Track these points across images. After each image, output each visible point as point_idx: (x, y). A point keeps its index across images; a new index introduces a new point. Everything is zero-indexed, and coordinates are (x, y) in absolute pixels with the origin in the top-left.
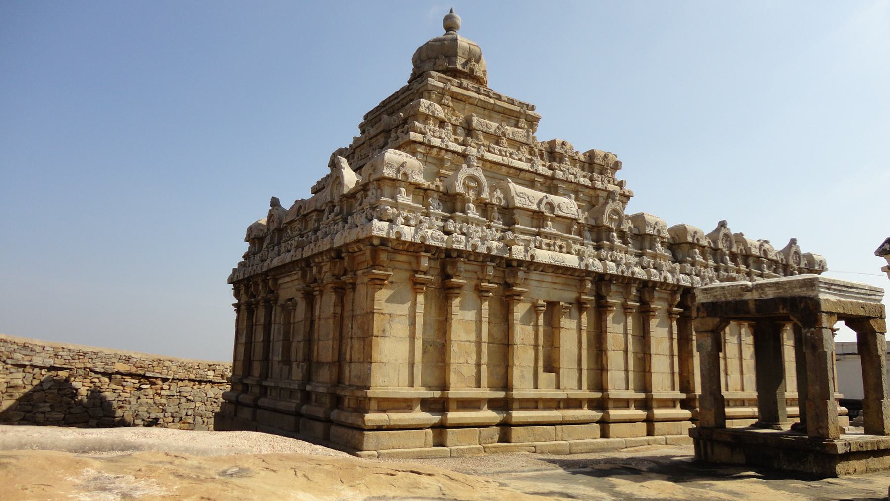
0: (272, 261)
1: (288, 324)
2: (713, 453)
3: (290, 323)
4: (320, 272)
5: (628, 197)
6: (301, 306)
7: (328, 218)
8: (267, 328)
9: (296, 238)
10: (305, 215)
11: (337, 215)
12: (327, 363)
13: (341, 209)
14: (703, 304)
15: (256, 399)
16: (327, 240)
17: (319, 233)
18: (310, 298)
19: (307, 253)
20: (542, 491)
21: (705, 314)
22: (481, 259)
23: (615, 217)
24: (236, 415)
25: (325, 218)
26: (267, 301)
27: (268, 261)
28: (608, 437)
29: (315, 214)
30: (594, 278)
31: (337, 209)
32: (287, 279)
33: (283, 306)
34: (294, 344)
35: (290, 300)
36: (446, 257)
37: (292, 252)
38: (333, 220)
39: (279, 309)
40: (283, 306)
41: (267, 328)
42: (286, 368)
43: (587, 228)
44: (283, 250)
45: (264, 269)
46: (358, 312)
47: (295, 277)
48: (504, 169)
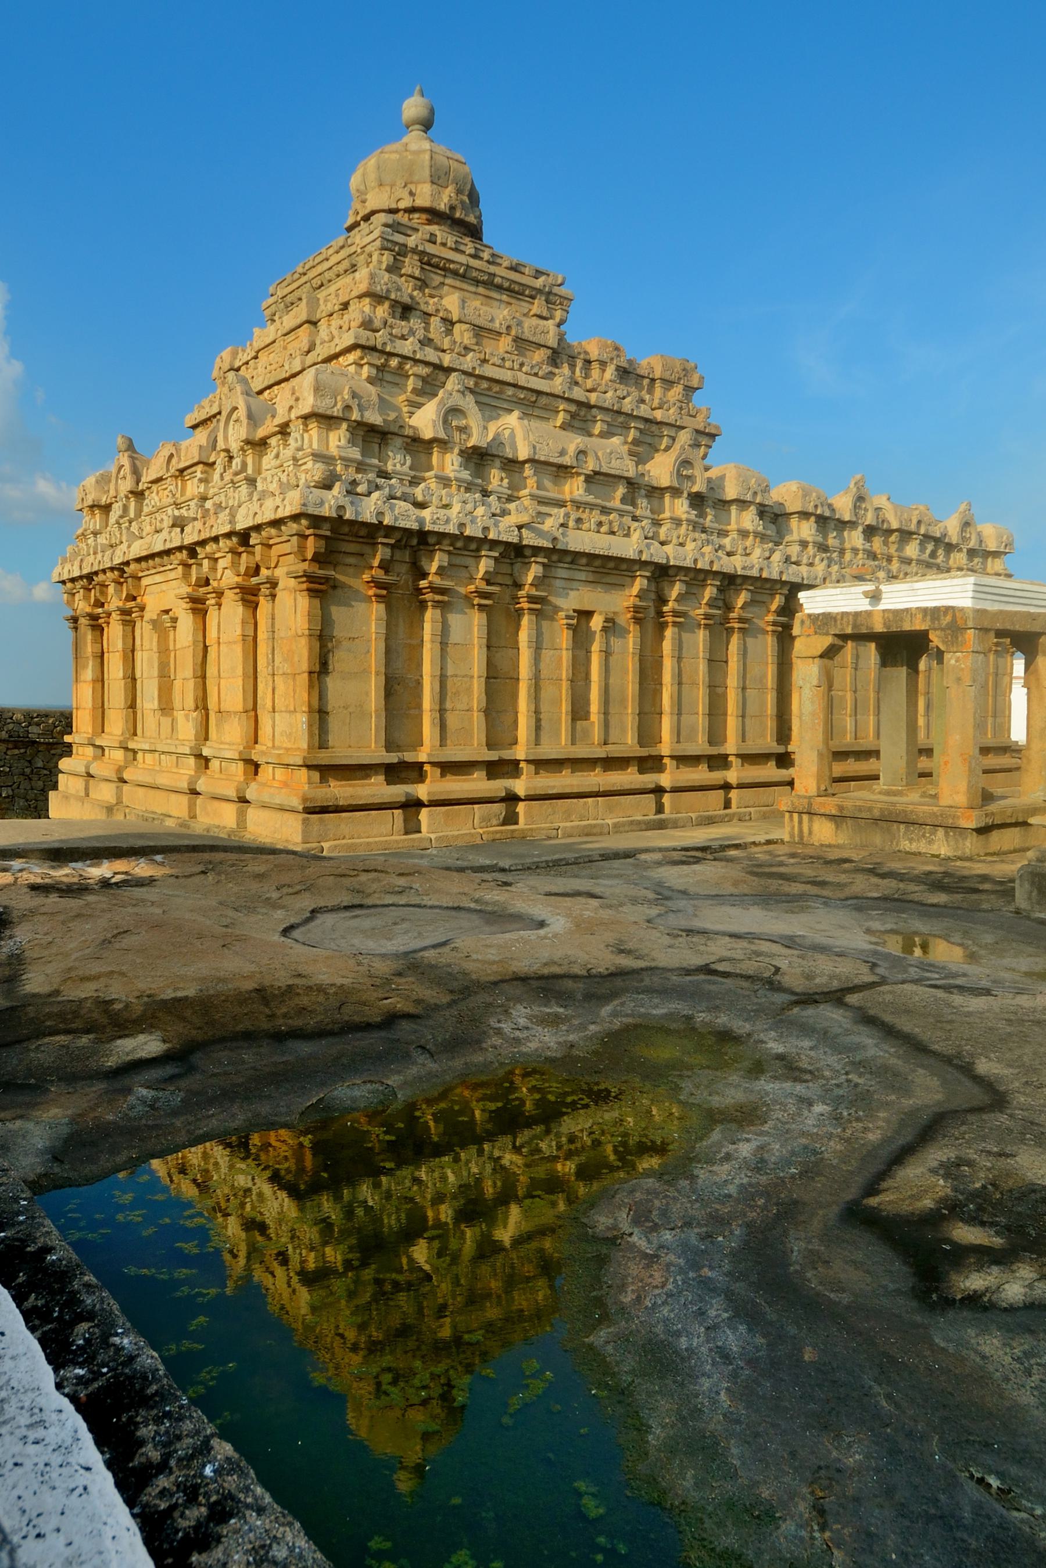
0: (129, 547)
1: (164, 651)
2: (810, 833)
3: (167, 649)
4: (214, 569)
5: (713, 436)
6: (186, 621)
7: (222, 478)
8: (130, 654)
9: (169, 510)
10: (182, 471)
11: (236, 474)
12: (235, 713)
13: (244, 465)
14: (809, 615)
15: (120, 770)
16: (224, 516)
17: (208, 504)
18: (198, 606)
19: (191, 536)
20: (562, 891)
21: (811, 631)
22: (473, 546)
23: (256, 1139)
24: (87, 795)
25: (216, 476)
26: (125, 612)
27: (124, 547)
28: (65, 721)
29: (200, 468)
30: (653, 573)
31: (237, 463)
32: (158, 578)
33: (154, 623)
34: (177, 684)
35: (167, 612)
36: (419, 544)
37: (164, 534)
38: (232, 482)
39: (148, 627)
40: (154, 623)
41: (130, 654)
42: (166, 721)
43: (643, 492)
44: (148, 529)
45: (117, 561)
46: (282, 634)
47: (172, 575)
48: (510, 391)
